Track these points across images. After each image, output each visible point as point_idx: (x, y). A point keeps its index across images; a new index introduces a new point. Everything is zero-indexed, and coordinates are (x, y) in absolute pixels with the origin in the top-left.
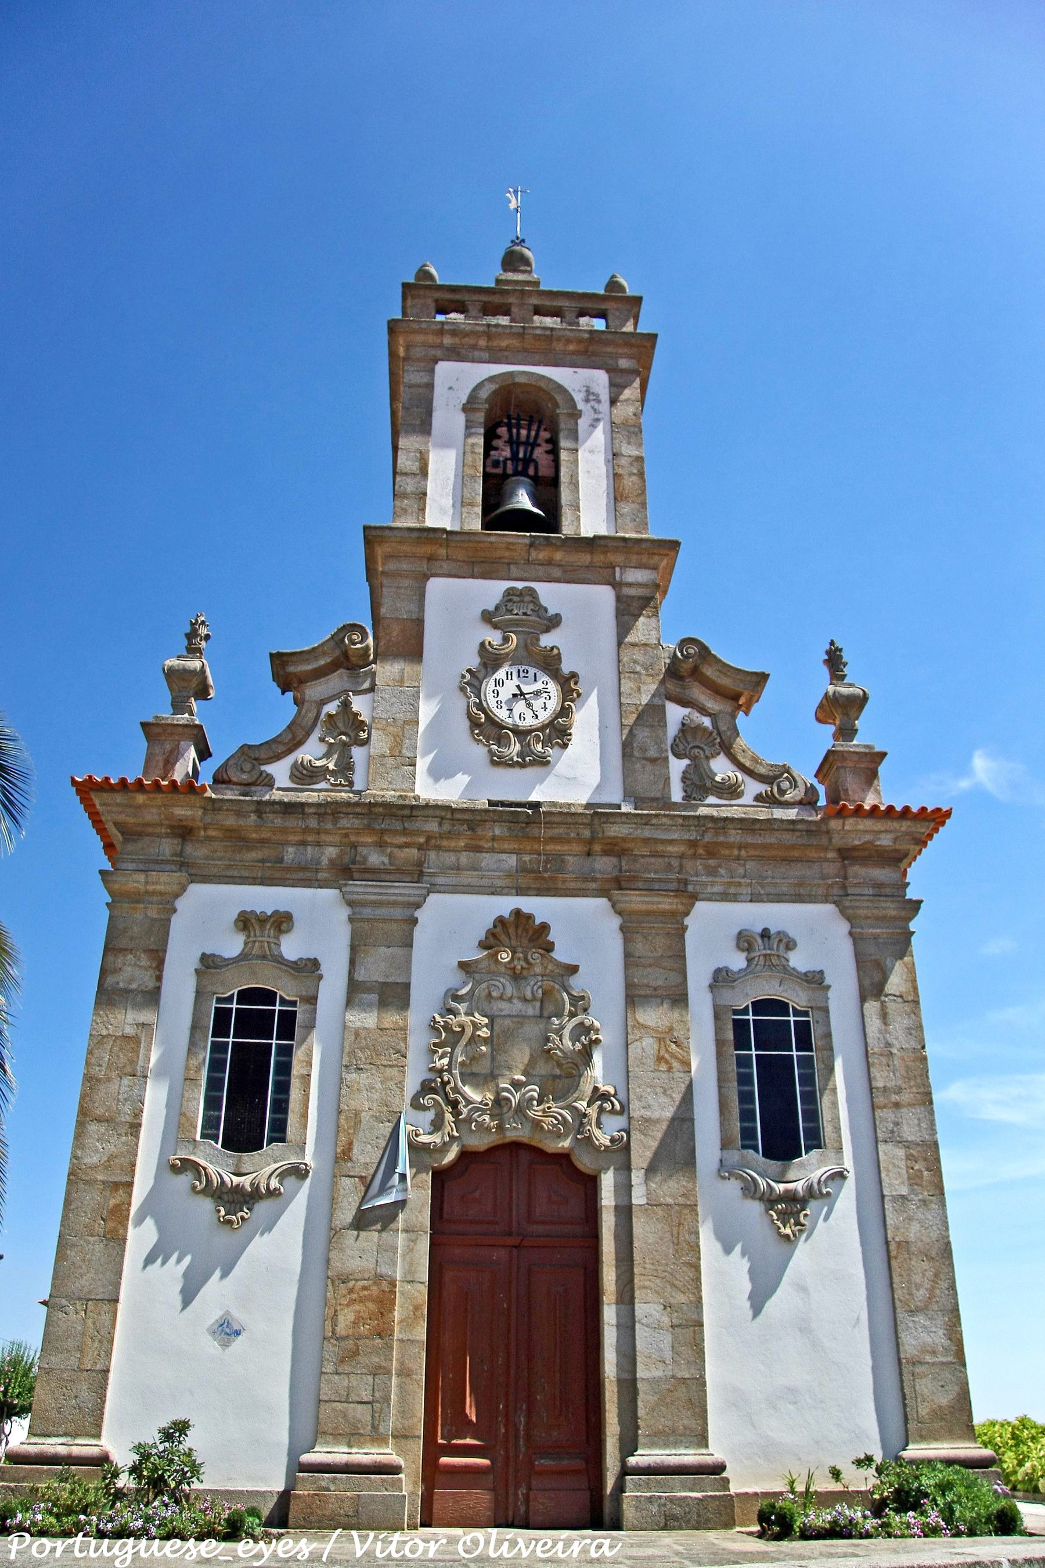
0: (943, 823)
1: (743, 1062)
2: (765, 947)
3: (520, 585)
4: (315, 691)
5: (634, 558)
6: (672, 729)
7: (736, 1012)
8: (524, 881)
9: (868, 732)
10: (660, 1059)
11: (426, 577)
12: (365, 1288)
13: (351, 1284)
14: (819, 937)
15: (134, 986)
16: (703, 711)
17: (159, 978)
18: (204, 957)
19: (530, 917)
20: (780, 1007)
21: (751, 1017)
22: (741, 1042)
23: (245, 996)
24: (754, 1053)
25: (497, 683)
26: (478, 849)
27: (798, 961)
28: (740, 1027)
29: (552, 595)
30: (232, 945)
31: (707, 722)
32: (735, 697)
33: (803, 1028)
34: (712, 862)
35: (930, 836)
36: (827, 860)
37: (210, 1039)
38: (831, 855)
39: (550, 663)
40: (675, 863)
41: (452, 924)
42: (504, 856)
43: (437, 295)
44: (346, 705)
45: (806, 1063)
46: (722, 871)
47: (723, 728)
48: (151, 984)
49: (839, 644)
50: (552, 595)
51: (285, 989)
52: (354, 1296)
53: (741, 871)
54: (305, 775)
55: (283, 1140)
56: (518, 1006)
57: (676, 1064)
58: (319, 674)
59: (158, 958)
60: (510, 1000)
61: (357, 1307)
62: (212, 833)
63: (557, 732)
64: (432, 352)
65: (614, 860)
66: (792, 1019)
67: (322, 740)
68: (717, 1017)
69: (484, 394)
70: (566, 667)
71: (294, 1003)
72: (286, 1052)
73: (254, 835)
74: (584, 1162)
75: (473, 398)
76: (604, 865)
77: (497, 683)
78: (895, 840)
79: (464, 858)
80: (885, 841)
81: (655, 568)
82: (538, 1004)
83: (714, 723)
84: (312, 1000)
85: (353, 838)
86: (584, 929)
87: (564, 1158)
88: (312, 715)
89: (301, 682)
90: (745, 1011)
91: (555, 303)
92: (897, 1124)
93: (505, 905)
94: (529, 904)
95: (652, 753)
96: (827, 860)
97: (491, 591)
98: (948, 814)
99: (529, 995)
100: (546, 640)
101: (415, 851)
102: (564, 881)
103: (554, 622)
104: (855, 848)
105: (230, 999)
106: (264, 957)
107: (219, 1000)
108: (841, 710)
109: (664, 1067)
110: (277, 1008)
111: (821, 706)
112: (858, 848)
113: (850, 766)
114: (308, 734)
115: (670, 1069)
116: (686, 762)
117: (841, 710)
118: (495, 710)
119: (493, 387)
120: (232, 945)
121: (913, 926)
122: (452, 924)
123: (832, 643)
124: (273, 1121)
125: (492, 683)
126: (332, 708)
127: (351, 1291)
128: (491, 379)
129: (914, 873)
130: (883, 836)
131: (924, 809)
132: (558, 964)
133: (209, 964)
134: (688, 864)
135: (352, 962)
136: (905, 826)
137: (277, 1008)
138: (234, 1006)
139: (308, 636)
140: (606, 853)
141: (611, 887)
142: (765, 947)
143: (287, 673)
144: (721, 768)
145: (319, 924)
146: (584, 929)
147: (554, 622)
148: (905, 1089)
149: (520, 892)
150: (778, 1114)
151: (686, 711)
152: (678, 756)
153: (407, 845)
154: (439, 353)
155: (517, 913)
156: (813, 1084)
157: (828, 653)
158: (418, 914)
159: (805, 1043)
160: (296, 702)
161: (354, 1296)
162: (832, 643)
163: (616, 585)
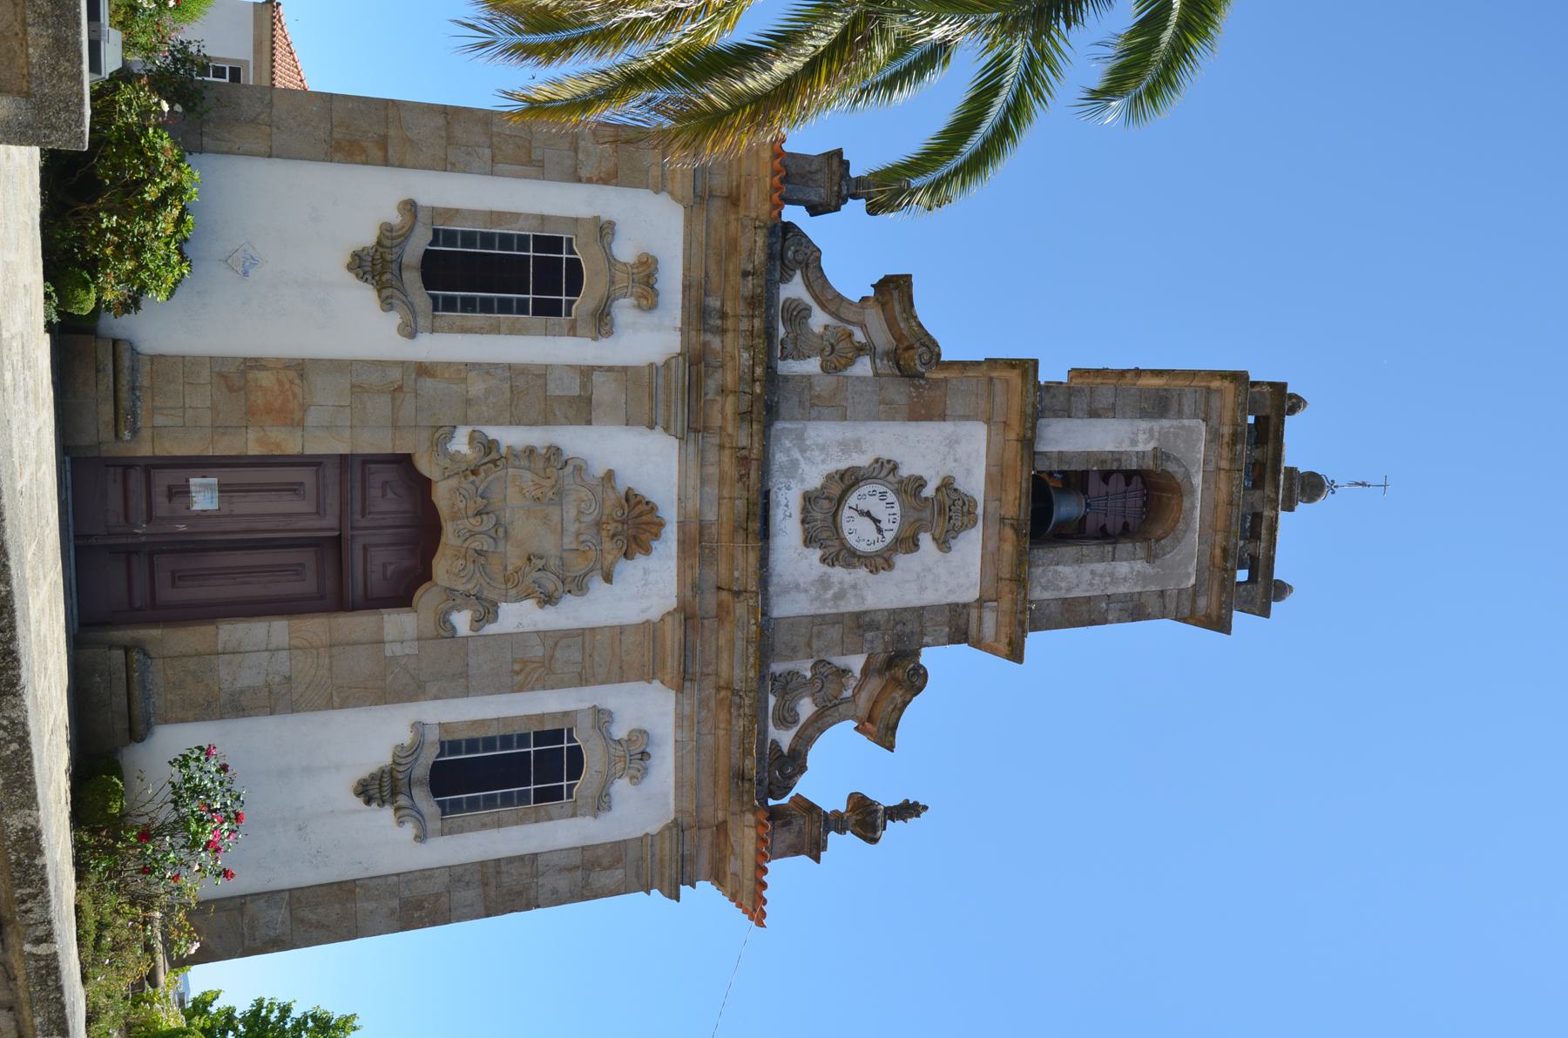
0: (751, 918)
1: (523, 739)
2: (635, 755)
3: (980, 511)
4: (874, 317)
5: (1006, 620)
6: (840, 661)
7: (570, 731)
8: (693, 528)
9: (841, 844)
10: (525, 662)
11: (988, 421)
12: (295, 395)
13: (297, 381)
14: (642, 807)
15: (581, 156)
16: (859, 688)
17: (589, 181)
18: (611, 224)
19: (657, 536)
20: (576, 773)
21: (565, 745)
22: (541, 737)
23: (575, 266)
24: (532, 749)
25: (883, 494)
26: (721, 482)
27: (621, 787)
28: (556, 736)
29: (971, 546)
30: (625, 251)
31: (848, 693)
32: (870, 719)
33: (556, 795)
34: (713, 703)
35: (740, 905)
36: (716, 810)
37: (211, 79)
38: (721, 815)
39: (907, 542)
40: (711, 669)
41: (648, 461)
42: (715, 509)
43: (1273, 420)
44: (860, 350)
45: (523, 798)
46: (704, 713)
47: (841, 708)
48: (584, 173)
49: (923, 815)
50: (971, 546)
51: (583, 303)
52: (287, 386)
53: (705, 731)
54: (796, 314)
55: (435, 309)
56: (572, 528)
57: (520, 678)
58: (891, 323)
59: (610, 178)
60: (578, 520)
61: (276, 388)
62: (733, 225)
63: (841, 554)
64: (1214, 416)
65: (713, 613)
66: (565, 783)
67: (826, 327)
68: (565, 714)
69: (1171, 467)
70: (901, 560)
71: (569, 314)
72: (522, 308)
73: (731, 267)
74: (426, 597)
75: (1168, 457)
76: (710, 600)
77: (883, 494)
78: (735, 874)
79: (713, 470)
80: (733, 866)
81: (996, 640)
82: (574, 546)
83: (845, 700)
84: (573, 331)
85: (730, 365)
86: (646, 589)
87: (426, 575)
88: (851, 317)
89: (883, 305)
90: (571, 739)
91: (1264, 532)
92: (468, 883)
93: (670, 513)
94: (671, 533)
95: (816, 644)
96: (716, 810)
97: (975, 484)
98: (760, 924)
99: (582, 538)
100: (926, 539)
101: (719, 423)
102: (692, 567)
103: (943, 544)
104: (726, 836)
105: (571, 251)
106: (612, 282)
107: (570, 241)
108: (866, 818)
109: (517, 667)
110: (564, 298)
111: (864, 798)
112: (751, 819)
113: (807, 831)
114: (831, 313)
115: (517, 673)
116: (809, 675)
117: (866, 818)
118: (856, 494)
119: (1179, 477)
120: (625, 251)
121: (655, 892)
122: (648, 461)
123: (925, 808)
124: (454, 298)
125: (883, 489)
126: (859, 336)
127: (291, 382)
128: (1188, 475)
129: (705, 887)
130: (739, 863)
131: (765, 902)
132: (613, 564)
133: (604, 230)
134: (709, 683)
135: (610, 369)
136: (749, 884)
137: (564, 298)
138: (564, 256)
139: (930, 311)
140: (720, 605)
141: (687, 614)
142: (635, 755)
143: (894, 289)
144: (806, 708)
145: (648, 339)
146: (646, 589)
147: (943, 544)
148: (503, 890)
149: (682, 525)
150: (468, 776)
151: (857, 673)
152: (814, 667)
153: (724, 417)
154: (1214, 422)
155: (661, 524)
156: (503, 805)
157: (916, 804)
158: (659, 429)
159: (541, 796)
160: (864, 299)
161: (287, 386)
162: (925, 808)
163: (981, 602)
